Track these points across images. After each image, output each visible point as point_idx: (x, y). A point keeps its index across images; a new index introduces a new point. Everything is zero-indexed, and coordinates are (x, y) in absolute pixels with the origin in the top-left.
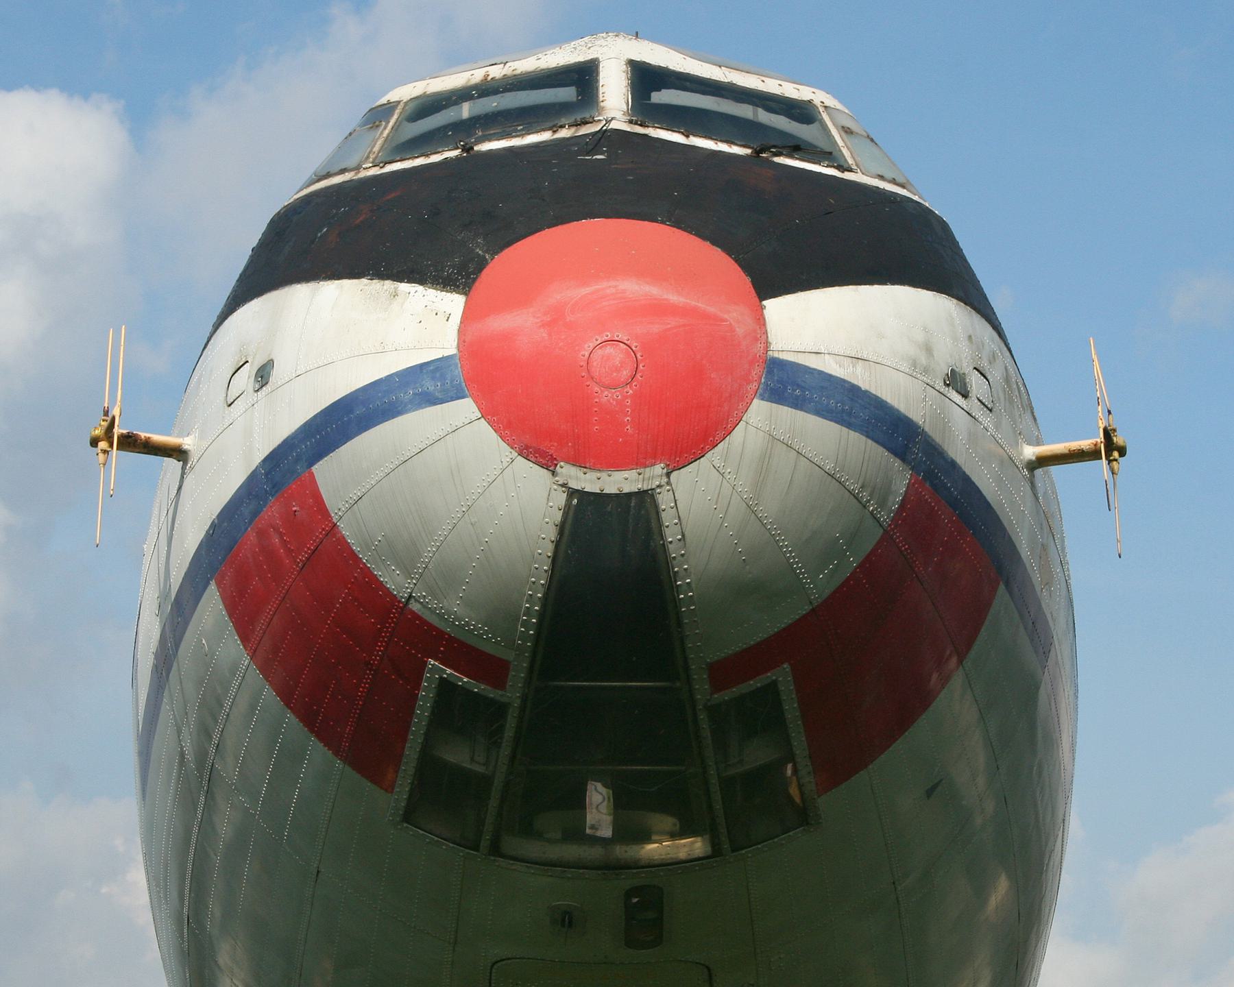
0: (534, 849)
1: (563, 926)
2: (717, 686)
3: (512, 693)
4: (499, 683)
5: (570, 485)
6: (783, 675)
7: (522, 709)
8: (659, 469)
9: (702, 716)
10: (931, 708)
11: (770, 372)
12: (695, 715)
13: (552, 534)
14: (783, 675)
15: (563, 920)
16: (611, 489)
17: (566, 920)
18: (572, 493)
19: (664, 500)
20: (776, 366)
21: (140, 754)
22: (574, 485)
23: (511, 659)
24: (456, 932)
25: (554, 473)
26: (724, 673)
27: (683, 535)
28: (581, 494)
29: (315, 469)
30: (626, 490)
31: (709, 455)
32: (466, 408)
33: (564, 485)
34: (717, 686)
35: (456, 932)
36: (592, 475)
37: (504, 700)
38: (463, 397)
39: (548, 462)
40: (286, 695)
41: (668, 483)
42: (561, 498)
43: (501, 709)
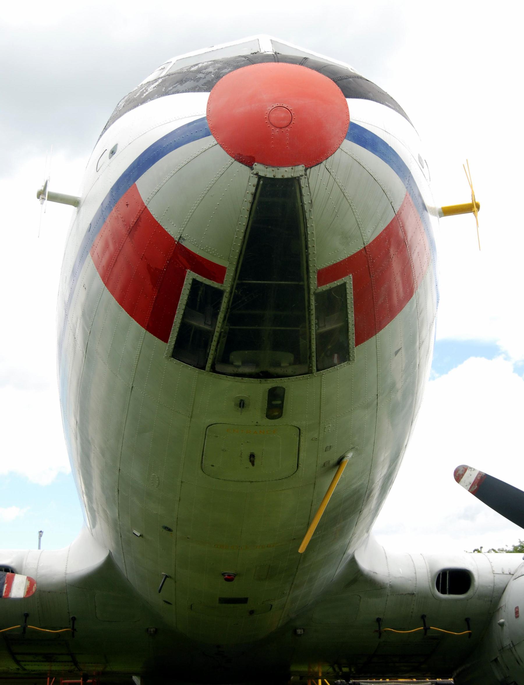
0: (230, 369)
1: (240, 407)
2: (321, 283)
3: (227, 285)
4: (221, 281)
5: (260, 174)
6: (349, 280)
7: (231, 293)
8: (301, 168)
9: (313, 298)
10: (403, 310)
11: (351, 129)
12: (309, 297)
13: (250, 198)
14: (349, 280)
15: (240, 404)
16: (279, 176)
17: (242, 404)
18: (260, 178)
19: (303, 182)
20: (354, 126)
21: (85, 479)
22: (261, 174)
23: (227, 266)
24: (192, 411)
25: (252, 169)
26: (326, 275)
27: (311, 201)
28: (265, 178)
29: (136, 183)
30: (286, 177)
31: (324, 162)
32: (211, 140)
33: (257, 174)
34: (321, 283)
35: (192, 411)
36: (270, 169)
37: (222, 288)
38: (209, 135)
39: (248, 161)
40: (121, 301)
41: (306, 175)
42: (255, 180)
43: (219, 293)
